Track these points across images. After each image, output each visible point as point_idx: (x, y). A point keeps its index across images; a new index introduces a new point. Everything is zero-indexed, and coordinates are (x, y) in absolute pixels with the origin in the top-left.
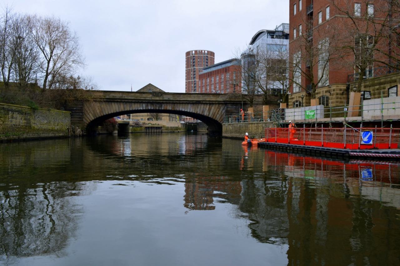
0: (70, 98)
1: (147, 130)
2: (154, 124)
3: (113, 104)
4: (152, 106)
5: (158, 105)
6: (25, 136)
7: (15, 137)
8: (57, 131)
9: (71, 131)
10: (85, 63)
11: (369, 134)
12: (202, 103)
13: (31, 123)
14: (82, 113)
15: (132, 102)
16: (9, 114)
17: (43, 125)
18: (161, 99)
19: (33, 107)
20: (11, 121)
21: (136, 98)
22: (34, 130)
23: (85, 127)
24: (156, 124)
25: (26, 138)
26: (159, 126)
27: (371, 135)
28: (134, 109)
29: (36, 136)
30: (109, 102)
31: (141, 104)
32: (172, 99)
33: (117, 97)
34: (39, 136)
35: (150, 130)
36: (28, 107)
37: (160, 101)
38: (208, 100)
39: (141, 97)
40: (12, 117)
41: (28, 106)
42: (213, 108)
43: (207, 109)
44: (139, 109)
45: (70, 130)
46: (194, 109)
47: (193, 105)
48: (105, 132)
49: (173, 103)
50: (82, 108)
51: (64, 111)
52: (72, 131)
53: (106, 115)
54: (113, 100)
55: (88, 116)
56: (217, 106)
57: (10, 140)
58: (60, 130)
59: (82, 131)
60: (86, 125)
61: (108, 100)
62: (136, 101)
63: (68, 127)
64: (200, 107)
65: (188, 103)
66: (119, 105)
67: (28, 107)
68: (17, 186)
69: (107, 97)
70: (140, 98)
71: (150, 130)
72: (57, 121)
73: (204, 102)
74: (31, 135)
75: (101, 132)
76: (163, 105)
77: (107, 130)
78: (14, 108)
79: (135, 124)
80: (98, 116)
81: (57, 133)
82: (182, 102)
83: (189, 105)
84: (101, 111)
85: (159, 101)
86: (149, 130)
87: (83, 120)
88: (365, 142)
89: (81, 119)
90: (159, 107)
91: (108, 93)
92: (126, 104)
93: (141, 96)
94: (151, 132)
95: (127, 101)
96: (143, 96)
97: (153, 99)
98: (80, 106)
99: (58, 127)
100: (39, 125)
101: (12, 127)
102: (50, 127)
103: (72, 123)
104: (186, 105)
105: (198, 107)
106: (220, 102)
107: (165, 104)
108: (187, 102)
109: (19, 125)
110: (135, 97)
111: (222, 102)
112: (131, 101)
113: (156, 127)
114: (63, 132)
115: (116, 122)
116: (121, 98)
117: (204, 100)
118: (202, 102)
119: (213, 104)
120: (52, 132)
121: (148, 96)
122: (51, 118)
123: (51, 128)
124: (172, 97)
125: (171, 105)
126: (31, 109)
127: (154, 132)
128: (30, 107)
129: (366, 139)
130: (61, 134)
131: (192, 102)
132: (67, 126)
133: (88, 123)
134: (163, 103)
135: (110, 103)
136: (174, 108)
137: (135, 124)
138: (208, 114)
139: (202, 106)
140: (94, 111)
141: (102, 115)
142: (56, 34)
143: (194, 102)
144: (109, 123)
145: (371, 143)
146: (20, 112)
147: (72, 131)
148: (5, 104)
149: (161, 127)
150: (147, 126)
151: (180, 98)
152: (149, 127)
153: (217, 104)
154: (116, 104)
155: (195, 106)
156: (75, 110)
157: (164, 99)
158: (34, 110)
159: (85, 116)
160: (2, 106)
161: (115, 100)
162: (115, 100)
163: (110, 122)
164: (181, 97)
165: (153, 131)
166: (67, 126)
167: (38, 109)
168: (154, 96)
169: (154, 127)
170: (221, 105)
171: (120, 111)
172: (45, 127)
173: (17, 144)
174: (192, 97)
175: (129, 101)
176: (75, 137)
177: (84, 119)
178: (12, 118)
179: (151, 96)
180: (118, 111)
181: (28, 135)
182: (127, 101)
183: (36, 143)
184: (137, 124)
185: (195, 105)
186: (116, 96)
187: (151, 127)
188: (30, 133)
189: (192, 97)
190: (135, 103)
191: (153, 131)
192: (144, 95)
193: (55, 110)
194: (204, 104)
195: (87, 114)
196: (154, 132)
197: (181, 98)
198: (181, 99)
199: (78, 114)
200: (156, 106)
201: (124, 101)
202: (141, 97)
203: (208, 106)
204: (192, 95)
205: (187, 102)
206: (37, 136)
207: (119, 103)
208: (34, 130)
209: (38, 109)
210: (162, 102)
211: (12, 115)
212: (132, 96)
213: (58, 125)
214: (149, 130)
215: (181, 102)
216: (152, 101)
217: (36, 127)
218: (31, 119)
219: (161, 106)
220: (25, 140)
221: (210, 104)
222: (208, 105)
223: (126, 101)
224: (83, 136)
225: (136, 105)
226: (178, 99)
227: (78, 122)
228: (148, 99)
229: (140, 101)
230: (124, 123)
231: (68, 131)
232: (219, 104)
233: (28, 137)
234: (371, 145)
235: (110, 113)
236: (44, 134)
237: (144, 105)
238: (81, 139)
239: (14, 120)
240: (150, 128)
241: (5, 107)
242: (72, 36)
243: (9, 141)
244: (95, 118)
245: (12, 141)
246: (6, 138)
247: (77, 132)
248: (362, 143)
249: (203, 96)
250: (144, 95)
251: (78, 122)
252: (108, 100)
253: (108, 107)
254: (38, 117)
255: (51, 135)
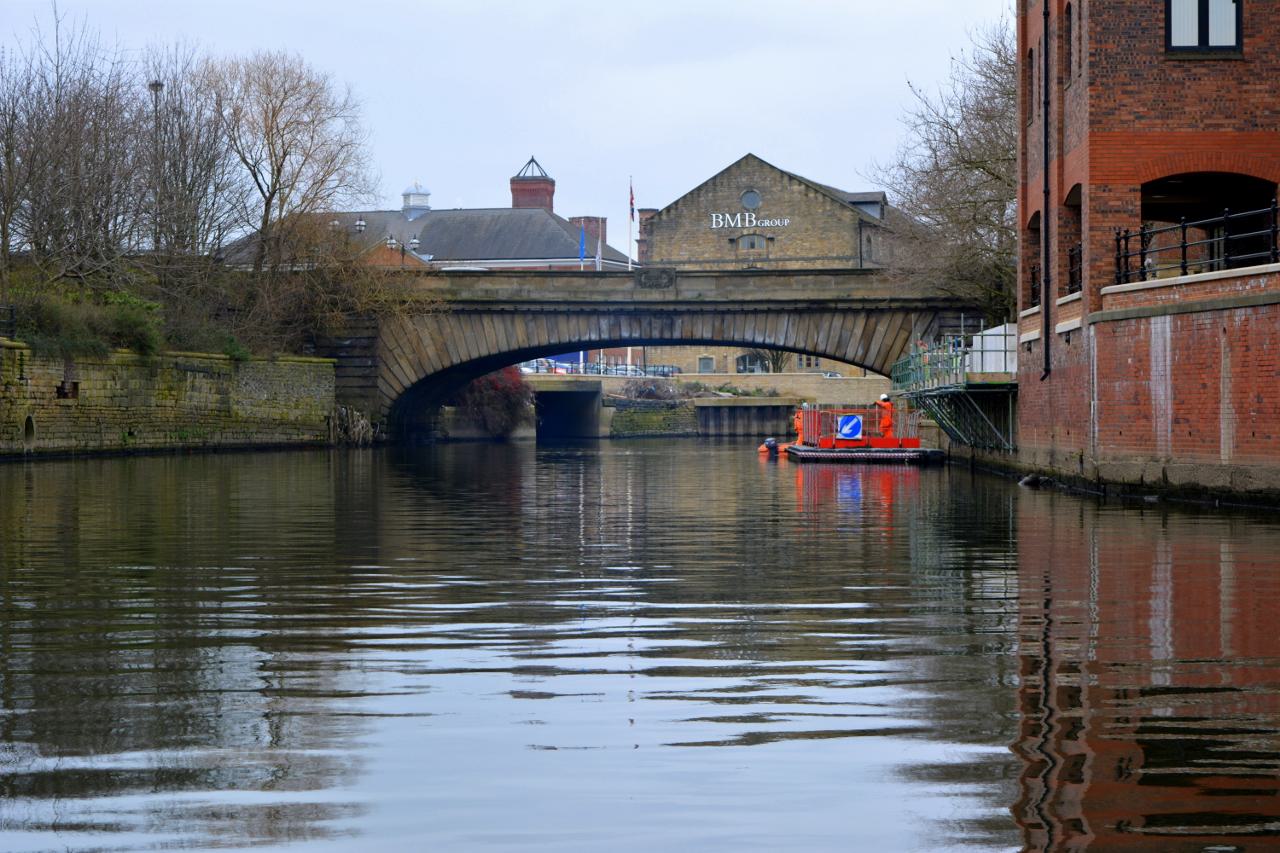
0: (318, 291)
1: (706, 426)
2: (752, 389)
3: (486, 320)
4: (635, 325)
5: (657, 323)
6: (217, 439)
7: (197, 440)
8: (295, 425)
9: (335, 425)
10: (382, 193)
11: (855, 421)
12: (835, 311)
13: (231, 400)
14: (373, 357)
15: (556, 313)
16: (186, 380)
17: (260, 406)
18: (671, 297)
19: (237, 353)
20: (191, 398)
21: (572, 298)
22: (237, 422)
23: (385, 411)
24: (759, 391)
25: (219, 444)
26: (776, 402)
27: (859, 422)
28: (565, 339)
29: (241, 440)
30: (470, 313)
31: (594, 319)
32: (711, 296)
33: (503, 296)
34: (248, 441)
35: (726, 423)
36: (223, 356)
37: (665, 307)
38: (858, 295)
39: (592, 293)
40: (193, 388)
41: (223, 353)
42: (881, 329)
43: (858, 331)
44: (586, 338)
45: (332, 424)
46: (802, 335)
47: (797, 318)
48: (472, 432)
49: (715, 312)
50: (374, 338)
51: (315, 360)
52: (341, 426)
53: (462, 364)
54: (487, 307)
55: (395, 368)
56: (899, 318)
57: (189, 449)
58: (304, 424)
59: (374, 425)
60: (388, 402)
61: (467, 307)
62: (572, 308)
63: (326, 413)
64: (826, 325)
65: (779, 312)
66: (509, 323)
67: (223, 356)
68: (200, 589)
69: (465, 295)
70: (588, 298)
71: (726, 423)
72: (291, 392)
73: (840, 306)
74: (229, 438)
75: (452, 434)
76: (679, 322)
77: (483, 424)
78: (196, 362)
79: (641, 394)
80: (430, 371)
81: (296, 432)
82: (752, 307)
83: (784, 319)
84: (443, 349)
85: (659, 307)
86: (719, 426)
87: (376, 387)
88: (845, 435)
89: (370, 384)
90: (662, 332)
91: (468, 280)
92: (534, 319)
93: (590, 288)
94: (733, 435)
95: (538, 307)
96: (598, 288)
97: (638, 297)
98: (366, 333)
99: (298, 412)
100: (249, 407)
101: (192, 413)
102: (276, 414)
103: (341, 397)
104: (771, 317)
105: (818, 328)
106: (907, 305)
107: (686, 318)
108: (772, 306)
109: (206, 407)
110: (570, 292)
111: (919, 305)
112: (552, 308)
113: (761, 409)
114: (311, 427)
115: (521, 387)
116: (517, 298)
117: (844, 295)
118: (833, 305)
119: (882, 311)
120: (280, 429)
121: (620, 287)
122: (280, 385)
123: (278, 417)
124: (713, 287)
125: (708, 319)
126: (230, 359)
127: (748, 435)
128: (228, 357)
129: (846, 430)
130: (306, 437)
131: (791, 307)
132: (323, 409)
133: (394, 395)
134: (677, 313)
135: (475, 317)
136: (722, 331)
137: (641, 394)
138: (860, 352)
139: (838, 321)
140: (418, 349)
141: (447, 364)
142: (288, 100)
143: (799, 306)
144: (492, 392)
145: (859, 436)
146: (208, 373)
147: (341, 426)
148: (179, 353)
149: (790, 409)
150: (709, 401)
151: (746, 293)
152: (717, 409)
153: (898, 310)
154: (497, 320)
155: (808, 321)
156: (348, 346)
157: (680, 298)
158: (237, 361)
159: (382, 365)
160: (174, 360)
161: (495, 307)
162: (495, 307)
163: (496, 389)
164: (751, 288)
165: (740, 430)
166: (323, 409)
167: (246, 360)
168: (643, 285)
169: (747, 408)
170: (913, 317)
171: (514, 346)
172: (263, 412)
173: (201, 458)
174: (795, 287)
175: (547, 308)
176: (348, 445)
177: (380, 382)
178: (192, 390)
179: (629, 285)
180: (504, 348)
181: (224, 435)
182: (538, 307)
183: (241, 458)
184: (650, 394)
185: (806, 317)
186: (497, 291)
187: (733, 410)
188: (227, 430)
189: (795, 287)
190: (567, 313)
191: (740, 430)
192: (605, 285)
193: (290, 358)
194: (845, 312)
195: (391, 362)
196: (748, 435)
197: (751, 292)
198: (749, 297)
199: (357, 362)
200: (650, 324)
201: (525, 307)
202: (592, 293)
203: (861, 321)
204: (793, 280)
205: (772, 306)
206: (243, 441)
207: (508, 318)
208: (237, 422)
209: (246, 360)
210: (671, 308)
211: (193, 382)
212: (556, 290)
213: (296, 407)
214: (719, 426)
215: (746, 307)
216: (632, 307)
217: (241, 413)
218: (230, 389)
219: (672, 326)
220: (218, 449)
221: (869, 312)
222: (863, 315)
223: (533, 307)
224: (376, 444)
225: (573, 321)
226: (740, 297)
227: (358, 391)
228: (619, 298)
229: (587, 308)
230: (575, 389)
231: (328, 424)
232: (907, 311)
233: (223, 441)
234: (858, 440)
235: (475, 355)
236: (260, 436)
237: (604, 323)
238: (370, 452)
239: (196, 394)
240: (710, 410)
241: (180, 360)
242: (341, 101)
243: (187, 451)
244: (422, 376)
245: (192, 452)
246: (181, 444)
247: (356, 430)
248: (839, 436)
249: (840, 278)
250: (602, 281)
251: (358, 391)
252: (467, 307)
253: (468, 333)
254: (246, 383)
255: (278, 437)
